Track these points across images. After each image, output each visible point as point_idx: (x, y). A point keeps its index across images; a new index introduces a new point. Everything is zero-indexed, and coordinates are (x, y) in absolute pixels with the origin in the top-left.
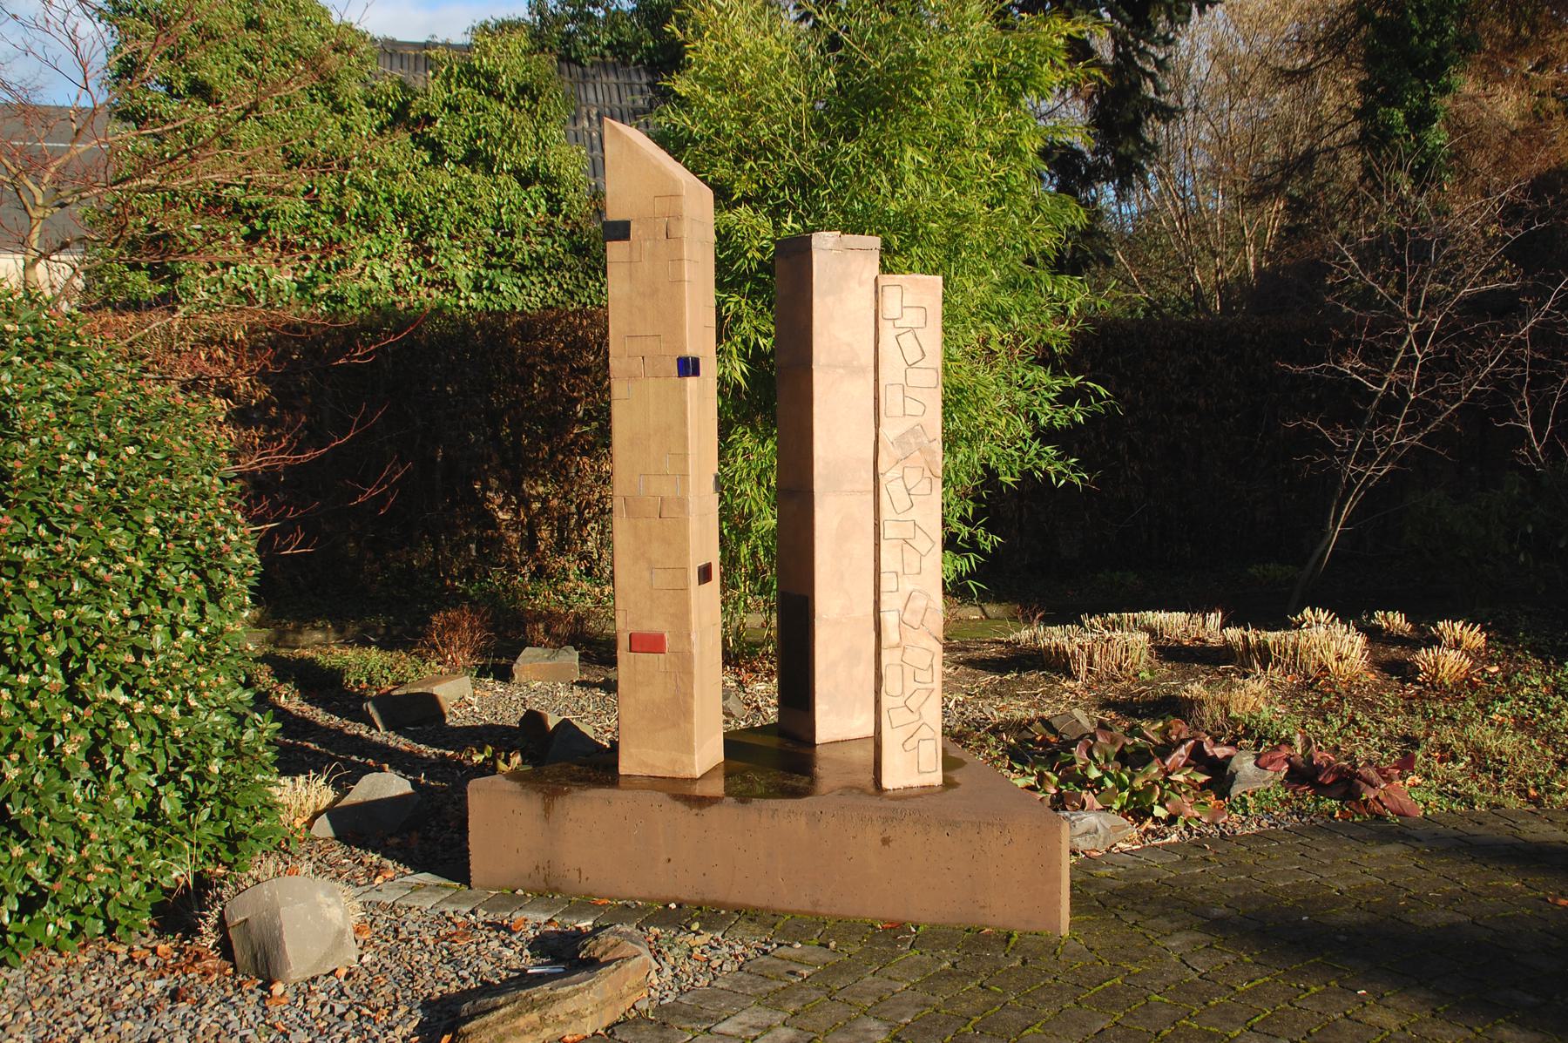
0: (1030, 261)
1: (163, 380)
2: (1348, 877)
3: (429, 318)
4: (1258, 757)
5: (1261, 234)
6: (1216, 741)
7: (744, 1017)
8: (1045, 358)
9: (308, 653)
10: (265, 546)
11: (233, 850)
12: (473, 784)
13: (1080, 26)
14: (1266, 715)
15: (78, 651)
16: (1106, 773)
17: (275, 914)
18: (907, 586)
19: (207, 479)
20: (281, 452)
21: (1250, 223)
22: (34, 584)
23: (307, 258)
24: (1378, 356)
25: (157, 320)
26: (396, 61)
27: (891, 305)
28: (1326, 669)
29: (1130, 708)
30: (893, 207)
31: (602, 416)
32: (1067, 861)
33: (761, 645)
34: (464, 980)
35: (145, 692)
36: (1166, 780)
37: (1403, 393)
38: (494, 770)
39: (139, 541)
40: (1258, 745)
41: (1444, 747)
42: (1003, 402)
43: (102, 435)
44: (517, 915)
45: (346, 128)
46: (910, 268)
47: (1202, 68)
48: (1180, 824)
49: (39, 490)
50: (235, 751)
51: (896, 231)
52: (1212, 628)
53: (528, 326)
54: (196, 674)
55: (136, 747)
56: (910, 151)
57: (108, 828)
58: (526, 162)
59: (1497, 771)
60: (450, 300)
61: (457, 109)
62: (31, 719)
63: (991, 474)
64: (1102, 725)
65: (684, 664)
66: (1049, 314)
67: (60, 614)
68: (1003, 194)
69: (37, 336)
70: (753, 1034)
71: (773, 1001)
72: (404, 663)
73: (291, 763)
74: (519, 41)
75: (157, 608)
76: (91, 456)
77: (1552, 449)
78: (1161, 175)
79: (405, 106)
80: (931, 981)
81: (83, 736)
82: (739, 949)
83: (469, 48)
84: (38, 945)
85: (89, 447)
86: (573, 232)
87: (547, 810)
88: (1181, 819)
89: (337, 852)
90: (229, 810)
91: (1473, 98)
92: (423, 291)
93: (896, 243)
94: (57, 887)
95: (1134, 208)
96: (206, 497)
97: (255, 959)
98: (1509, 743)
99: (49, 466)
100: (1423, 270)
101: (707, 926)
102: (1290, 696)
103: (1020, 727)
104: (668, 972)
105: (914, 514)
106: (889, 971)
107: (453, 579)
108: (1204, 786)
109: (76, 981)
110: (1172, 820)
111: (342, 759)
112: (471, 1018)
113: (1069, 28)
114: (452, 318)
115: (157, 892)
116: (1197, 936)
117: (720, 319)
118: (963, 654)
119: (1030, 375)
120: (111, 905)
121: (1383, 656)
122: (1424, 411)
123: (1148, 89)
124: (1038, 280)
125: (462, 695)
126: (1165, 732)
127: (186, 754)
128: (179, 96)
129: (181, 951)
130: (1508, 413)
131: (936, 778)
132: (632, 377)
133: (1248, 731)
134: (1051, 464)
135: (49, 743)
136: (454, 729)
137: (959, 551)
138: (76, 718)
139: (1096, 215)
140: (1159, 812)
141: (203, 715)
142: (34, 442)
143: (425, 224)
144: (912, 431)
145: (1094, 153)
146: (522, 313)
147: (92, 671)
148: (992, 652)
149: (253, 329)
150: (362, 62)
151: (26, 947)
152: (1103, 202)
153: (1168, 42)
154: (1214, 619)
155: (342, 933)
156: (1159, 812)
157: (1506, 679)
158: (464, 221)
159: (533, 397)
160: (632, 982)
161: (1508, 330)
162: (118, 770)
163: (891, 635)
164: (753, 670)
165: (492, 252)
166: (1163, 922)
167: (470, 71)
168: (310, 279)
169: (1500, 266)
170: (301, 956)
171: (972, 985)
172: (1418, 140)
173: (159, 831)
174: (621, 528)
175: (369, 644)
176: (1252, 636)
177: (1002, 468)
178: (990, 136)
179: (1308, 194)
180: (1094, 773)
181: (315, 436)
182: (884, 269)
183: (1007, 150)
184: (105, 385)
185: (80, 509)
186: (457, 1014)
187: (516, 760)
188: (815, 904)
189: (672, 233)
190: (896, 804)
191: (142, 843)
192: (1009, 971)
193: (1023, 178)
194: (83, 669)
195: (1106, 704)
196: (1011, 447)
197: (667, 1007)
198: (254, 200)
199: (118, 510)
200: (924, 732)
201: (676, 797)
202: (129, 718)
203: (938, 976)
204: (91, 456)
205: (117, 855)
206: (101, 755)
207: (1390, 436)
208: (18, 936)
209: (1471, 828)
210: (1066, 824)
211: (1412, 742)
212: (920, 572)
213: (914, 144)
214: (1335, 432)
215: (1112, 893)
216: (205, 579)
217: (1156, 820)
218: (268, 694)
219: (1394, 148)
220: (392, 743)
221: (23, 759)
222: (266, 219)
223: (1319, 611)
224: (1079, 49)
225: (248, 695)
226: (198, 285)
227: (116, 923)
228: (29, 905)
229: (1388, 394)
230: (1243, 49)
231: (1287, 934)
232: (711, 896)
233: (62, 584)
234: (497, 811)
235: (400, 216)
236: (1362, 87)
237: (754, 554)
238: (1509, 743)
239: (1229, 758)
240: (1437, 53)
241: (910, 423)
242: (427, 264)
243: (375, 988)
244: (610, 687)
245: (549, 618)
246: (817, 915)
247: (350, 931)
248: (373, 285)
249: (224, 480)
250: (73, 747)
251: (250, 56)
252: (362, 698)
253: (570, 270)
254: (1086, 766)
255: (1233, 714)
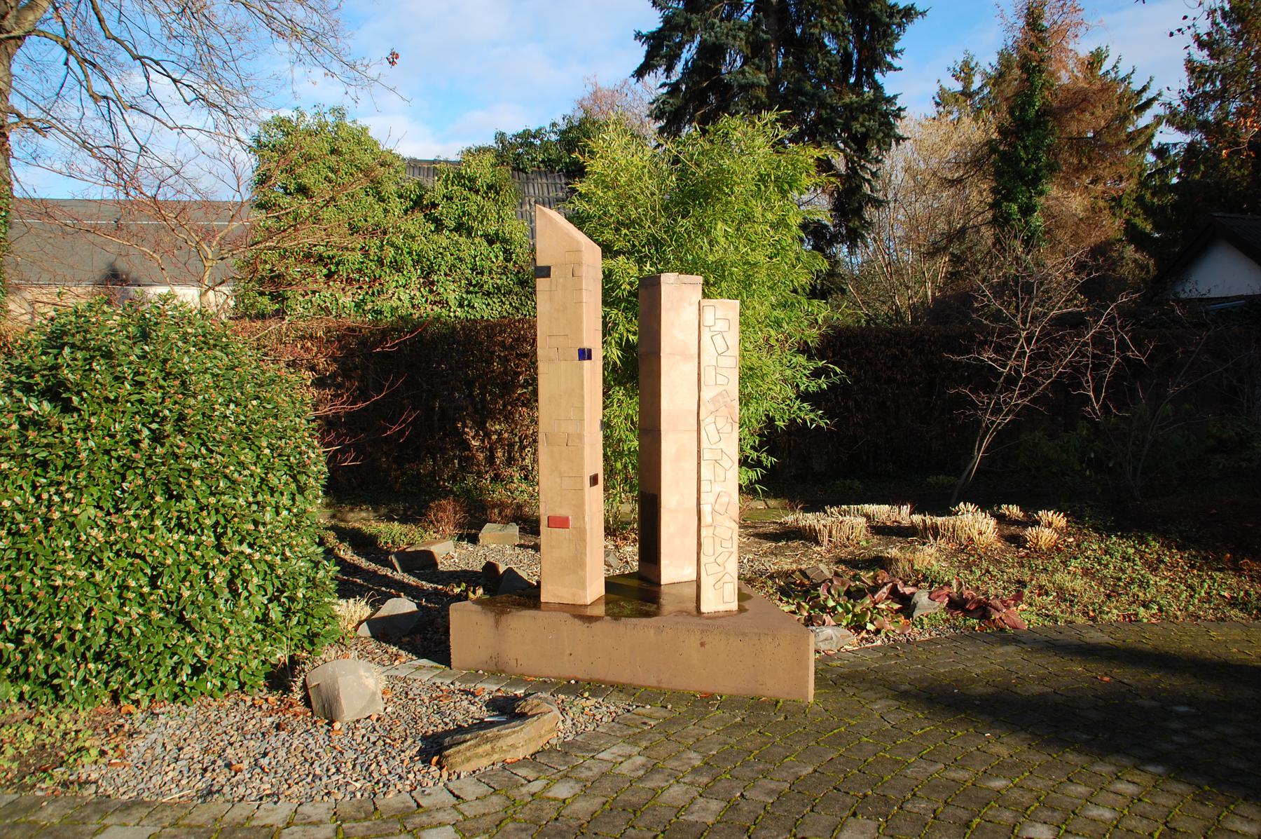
0: (795, 291)
1: (275, 361)
2: (982, 665)
3: (431, 323)
4: (930, 593)
5: (935, 277)
6: (905, 584)
7: (614, 749)
8: (804, 349)
9: (357, 525)
10: (331, 460)
11: (312, 643)
12: (453, 606)
13: (828, 152)
14: (936, 568)
15: (223, 522)
16: (838, 603)
17: (336, 681)
18: (718, 488)
19: (298, 420)
20: (343, 403)
21: (928, 269)
22: (198, 482)
23: (361, 288)
24: (1003, 350)
25: (273, 325)
26: (417, 172)
27: (708, 317)
28: (972, 540)
29: (853, 563)
30: (711, 258)
31: (533, 382)
32: (812, 657)
33: (629, 524)
34: (446, 724)
35: (261, 547)
36: (875, 608)
37: (1018, 373)
38: (466, 598)
39: (258, 456)
40: (931, 586)
41: (1041, 587)
42: (777, 375)
43: (238, 394)
44: (479, 686)
45: (386, 211)
46: (720, 294)
47: (899, 177)
48: (883, 634)
49: (202, 426)
50: (312, 583)
51: (713, 272)
52: (904, 515)
53: (491, 329)
54: (290, 537)
55: (255, 580)
56: (720, 225)
57: (240, 627)
58: (492, 230)
59: (1072, 601)
60: (444, 312)
61: (451, 199)
62: (196, 562)
63: (771, 420)
64: (836, 574)
65: (581, 534)
66: (806, 323)
67: (213, 500)
68: (777, 251)
69: (204, 336)
70: (620, 760)
71: (633, 740)
72: (413, 531)
73: (346, 591)
74: (489, 159)
75: (268, 497)
76: (232, 406)
77: (1104, 407)
78: (875, 241)
79: (421, 197)
80: (729, 729)
81: (226, 572)
82: (612, 709)
83: (459, 163)
84: (202, 694)
85: (231, 401)
86: (519, 272)
87: (497, 622)
88: (883, 632)
89: (373, 645)
90: (310, 619)
91: (1057, 199)
92: (429, 307)
93: (712, 280)
94: (211, 662)
95: (860, 260)
96: (297, 431)
97: (324, 708)
98: (1079, 584)
99: (208, 412)
100: (1030, 300)
101: (593, 695)
102: (950, 556)
103: (787, 574)
104: (569, 722)
105: (722, 445)
106: (704, 723)
107: (444, 481)
108: (897, 611)
109: (223, 716)
110: (878, 631)
111: (377, 590)
112: (451, 747)
113: (817, 153)
114: (445, 324)
115: (268, 665)
116: (891, 702)
117: (605, 324)
118: (751, 529)
119: (794, 360)
120: (241, 673)
121: (1006, 532)
122: (1031, 384)
123: (866, 188)
124: (799, 302)
125: (449, 552)
126: (875, 578)
127: (284, 585)
128: (290, 194)
129: (282, 701)
130: (1080, 386)
131: (734, 606)
132: (551, 360)
133: (925, 578)
134: (808, 415)
135: (206, 576)
136: (443, 572)
137: (751, 467)
138: (221, 562)
139: (835, 263)
140: (870, 627)
141: (294, 561)
142: (200, 398)
143: (431, 267)
144: (720, 394)
145: (834, 226)
146: (488, 320)
147: (230, 533)
148: (771, 529)
149: (328, 330)
150: (396, 172)
151: (195, 695)
152: (841, 255)
153: (878, 161)
154: (906, 509)
155: (374, 694)
156: (870, 627)
157: (1078, 546)
158: (453, 265)
159: (493, 371)
160: (547, 727)
161: (1079, 336)
162: (245, 594)
163: (707, 519)
164: (625, 539)
165: (470, 284)
166: (871, 694)
167: (460, 176)
168: (362, 301)
169: (1075, 298)
170: (349, 709)
171: (753, 732)
172: (1026, 222)
173: (269, 630)
174: (542, 448)
175: (394, 520)
176: (928, 519)
177: (777, 417)
178: (769, 216)
179: (963, 252)
180: (831, 603)
181: (363, 394)
182: (705, 295)
183: (781, 224)
184: (241, 364)
185: (224, 438)
186: (442, 744)
187: (480, 591)
188: (660, 682)
189: (576, 273)
190: (709, 621)
191: (259, 636)
192: (776, 724)
193: (790, 241)
194: (225, 533)
195: (840, 561)
196: (782, 403)
197: (568, 743)
198: (331, 253)
199: (246, 439)
200: (727, 578)
201: (575, 616)
202: (251, 562)
203: (733, 726)
204: (232, 406)
205: (245, 644)
206: (235, 584)
207: (1011, 399)
208: (191, 688)
209: (1055, 635)
210: (812, 635)
211: (1022, 584)
212: (724, 480)
213: (725, 221)
214: (978, 396)
215: (841, 676)
216: (294, 478)
217: (868, 632)
218: (333, 549)
219: (1012, 226)
220: (406, 581)
221: (192, 585)
222: (337, 264)
223: (968, 504)
224: (824, 165)
225: (321, 550)
226: (298, 304)
227: (245, 683)
228: (197, 670)
229: (1009, 374)
230: (922, 166)
231: (947, 700)
232: (596, 677)
233: (213, 482)
234: (467, 623)
235: (416, 263)
236: (994, 191)
237: (625, 467)
238: (1079, 584)
239: (913, 594)
240: (1036, 172)
241: (720, 389)
242: (431, 291)
243: (394, 727)
244: (537, 548)
245: (502, 506)
246: (660, 689)
247: (380, 694)
248: (399, 303)
249: (308, 422)
250: (220, 579)
251: (332, 170)
252: (388, 553)
253: (517, 294)
254: (827, 599)
255: (916, 567)
